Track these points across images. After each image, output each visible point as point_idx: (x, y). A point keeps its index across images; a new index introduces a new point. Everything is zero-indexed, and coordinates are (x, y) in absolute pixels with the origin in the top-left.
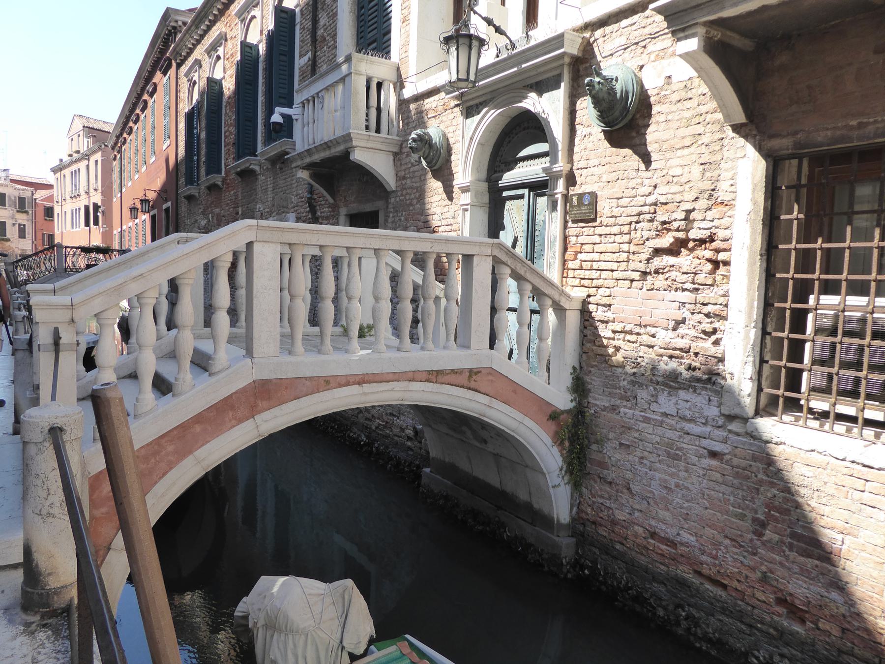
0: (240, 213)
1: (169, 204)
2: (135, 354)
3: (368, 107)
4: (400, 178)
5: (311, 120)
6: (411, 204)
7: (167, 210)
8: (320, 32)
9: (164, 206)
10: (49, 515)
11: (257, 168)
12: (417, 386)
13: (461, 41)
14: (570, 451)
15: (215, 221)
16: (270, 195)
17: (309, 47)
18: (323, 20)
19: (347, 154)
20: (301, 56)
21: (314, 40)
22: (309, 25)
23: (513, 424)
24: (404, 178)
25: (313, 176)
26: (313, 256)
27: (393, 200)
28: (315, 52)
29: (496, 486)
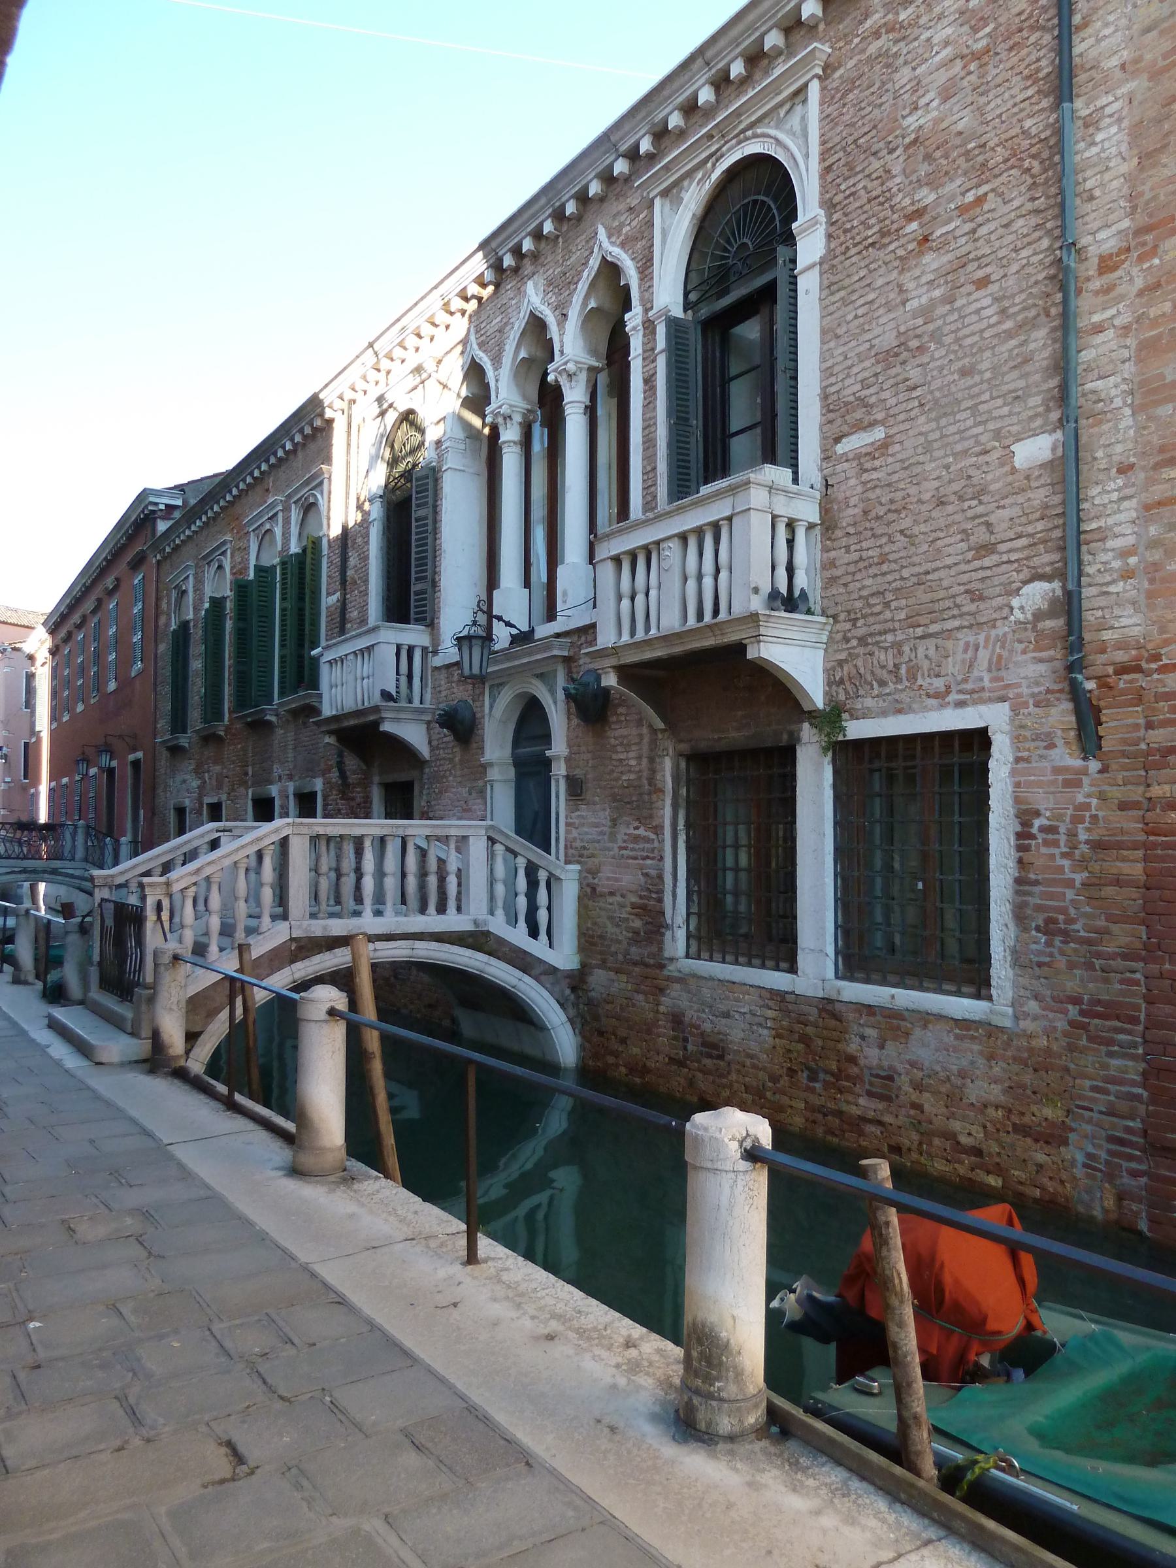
0: (250, 773)
1: (140, 754)
2: (204, 919)
3: (398, 673)
4: (433, 749)
5: (339, 683)
6: (444, 776)
7: (136, 764)
8: (350, 573)
9: (131, 757)
10: (171, 1009)
11: (273, 719)
12: (419, 944)
13: (474, 642)
14: (580, 1015)
15: (214, 783)
16: (290, 755)
17: (337, 585)
18: (352, 562)
19: (376, 724)
20: (329, 594)
21: (343, 582)
22: (337, 560)
23: (514, 981)
24: (438, 748)
25: (339, 740)
26: (483, 246)
27: (427, 770)
28: (345, 594)
29: (882, 1424)
